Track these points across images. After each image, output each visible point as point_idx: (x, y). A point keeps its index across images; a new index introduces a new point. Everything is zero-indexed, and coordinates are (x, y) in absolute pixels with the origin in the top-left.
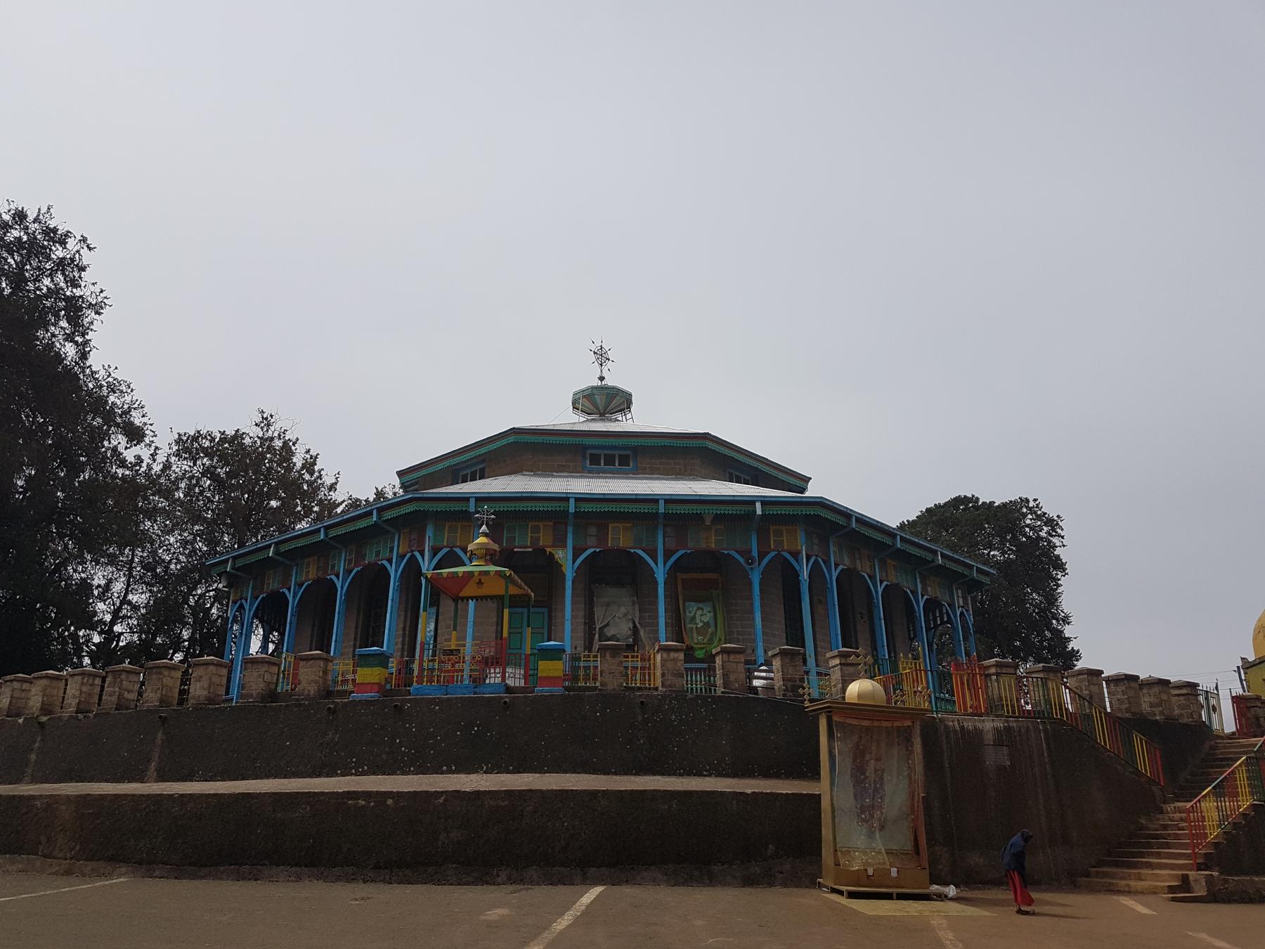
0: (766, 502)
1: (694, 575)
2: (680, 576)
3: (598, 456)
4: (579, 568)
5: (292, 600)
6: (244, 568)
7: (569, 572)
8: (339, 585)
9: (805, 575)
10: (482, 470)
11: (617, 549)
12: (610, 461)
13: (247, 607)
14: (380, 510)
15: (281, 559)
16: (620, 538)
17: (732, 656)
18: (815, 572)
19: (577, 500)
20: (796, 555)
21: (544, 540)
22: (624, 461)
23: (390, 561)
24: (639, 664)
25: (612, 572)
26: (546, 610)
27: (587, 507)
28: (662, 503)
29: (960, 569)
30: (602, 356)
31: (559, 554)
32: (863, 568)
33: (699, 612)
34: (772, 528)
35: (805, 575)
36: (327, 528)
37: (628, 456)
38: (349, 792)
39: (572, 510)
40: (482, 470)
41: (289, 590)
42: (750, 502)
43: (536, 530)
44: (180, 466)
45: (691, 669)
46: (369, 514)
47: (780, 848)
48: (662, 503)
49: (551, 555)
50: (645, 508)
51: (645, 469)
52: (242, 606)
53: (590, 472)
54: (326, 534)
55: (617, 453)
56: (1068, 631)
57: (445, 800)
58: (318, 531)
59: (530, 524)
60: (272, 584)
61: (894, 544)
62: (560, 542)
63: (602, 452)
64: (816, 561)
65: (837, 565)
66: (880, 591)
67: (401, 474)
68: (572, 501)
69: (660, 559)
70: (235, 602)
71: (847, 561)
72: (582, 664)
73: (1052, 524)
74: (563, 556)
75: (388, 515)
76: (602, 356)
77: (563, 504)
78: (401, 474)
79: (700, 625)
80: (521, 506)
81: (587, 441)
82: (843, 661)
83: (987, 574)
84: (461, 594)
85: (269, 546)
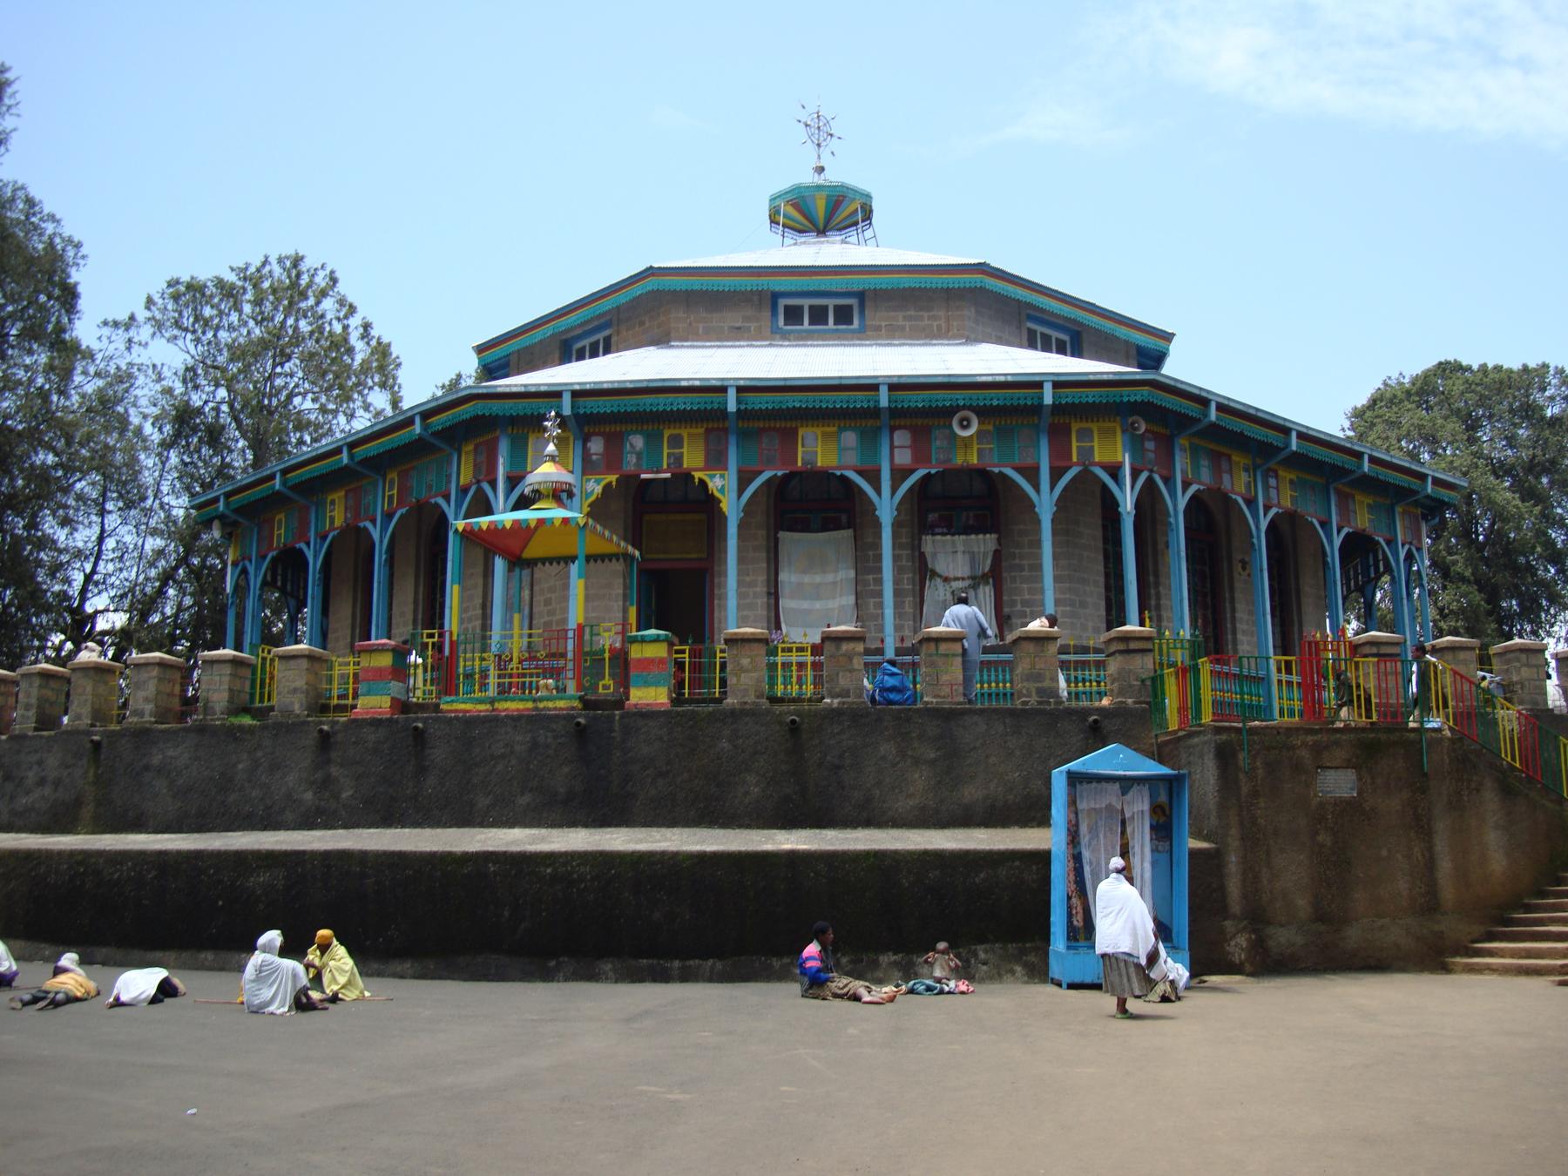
0: (1061, 383)
1: (662, 556)
5: (314, 559)
6: (366, 462)
7: (731, 506)
8: (376, 535)
9: (1128, 502)
11: (808, 473)
12: (818, 316)
13: (251, 570)
15: (290, 493)
16: (821, 451)
18: (1149, 502)
19: (740, 389)
20: (1114, 471)
21: (692, 458)
22: (844, 315)
23: (447, 497)
24: (810, 659)
25: (811, 507)
28: (884, 390)
30: (819, 131)
31: (715, 483)
32: (1237, 484)
34: (1075, 427)
35: (1128, 502)
37: (850, 307)
39: (732, 406)
40: (607, 341)
41: (308, 544)
42: (1032, 384)
43: (676, 441)
45: (989, 662)
47: (1003, 921)
48: (884, 390)
49: (702, 482)
50: (860, 400)
51: (878, 328)
52: (244, 571)
55: (830, 303)
58: (216, 500)
60: (281, 534)
61: (1288, 445)
62: (716, 461)
63: (806, 303)
64: (1150, 481)
65: (1186, 485)
66: (1264, 525)
67: (481, 349)
71: (1206, 475)
72: (779, 659)
74: (722, 485)
76: (819, 131)
77: (715, 396)
78: (481, 349)
80: (648, 402)
84: (527, 554)
85: (272, 477)
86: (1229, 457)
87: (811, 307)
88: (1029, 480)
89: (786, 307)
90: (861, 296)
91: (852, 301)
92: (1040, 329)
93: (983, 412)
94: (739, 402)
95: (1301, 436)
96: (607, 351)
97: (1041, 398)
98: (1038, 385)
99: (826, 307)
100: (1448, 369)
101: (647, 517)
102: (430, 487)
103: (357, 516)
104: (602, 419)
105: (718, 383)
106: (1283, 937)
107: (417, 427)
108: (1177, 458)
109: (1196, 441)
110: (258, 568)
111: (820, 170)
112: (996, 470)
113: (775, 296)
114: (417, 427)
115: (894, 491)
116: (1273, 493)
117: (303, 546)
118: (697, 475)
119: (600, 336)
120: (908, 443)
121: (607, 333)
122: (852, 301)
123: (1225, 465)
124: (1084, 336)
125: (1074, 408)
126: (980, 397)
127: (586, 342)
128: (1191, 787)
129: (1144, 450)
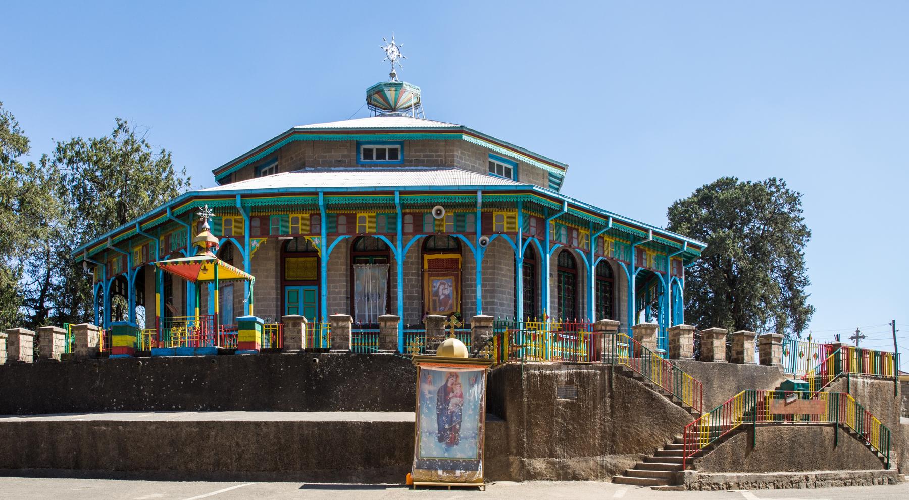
0: (486, 191)
2: (427, 257)
3: (371, 151)
4: (332, 253)
7: (324, 255)
10: (277, 167)
13: (103, 286)
14: (172, 208)
16: (367, 223)
17: (388, 324)
25: (365, 253)
26: (316, 288)
27: (333, 200)
29: (672, 244)
33: (442, 287)
36: (141, 223)
37: (397, 150)
38: (94, 422)
44: (63, 169)
45: (368, 333)
46: (163, 211)
50: (382, 199)
53: (363, 166)
54: (141, 229)
55: (387, 147)
56: (807, 290)
57: (157, 428)
59: (291, 216)
68: (397, 194)
69: (399, 243)
70: (96, 284)
73: (793, 200)
74: (319, 242)
75: (179, 210)
79: (442, 297)
81: (357, 137)
82: (478, 324)
83: (699, 248)
86: (577, 230)
87: (390, 150)
88: (239, 242)
89: (365, 150)
90: (402, 143)
91: (398, 147)
92: (496, 162)
93: (447, 206)
94: (324, 200)
95: (614, 220)
96: (276, 172)
97: (476, 199)
98: (392, 193)
99: (385, 150)
100: (726, 184)
101: (287, 259)
102: (178, 245)
103: (148, 260)
104: (264, 211)
105: (314, 191)
106: (806, 466)
107: (168, 214)
108: (548, 230)
109: (558, 221)
110: (106, 286)
111: (393, 75)
112: (376, 237)
113: (358, 144)
114: (168, 214)
115: (403, 248)
116: (601, 249)
117: (125, 274)
118: (306, 238)
119: (273, 165)
120: (411, 221)
121: (276, 163)
122: (398, 147)
123: (575, 234)
124: (520, 166)
125: (493, 203)
126: (441, 198)
127: (267, 168)
128: (661, 392)
129: (530, 226)
